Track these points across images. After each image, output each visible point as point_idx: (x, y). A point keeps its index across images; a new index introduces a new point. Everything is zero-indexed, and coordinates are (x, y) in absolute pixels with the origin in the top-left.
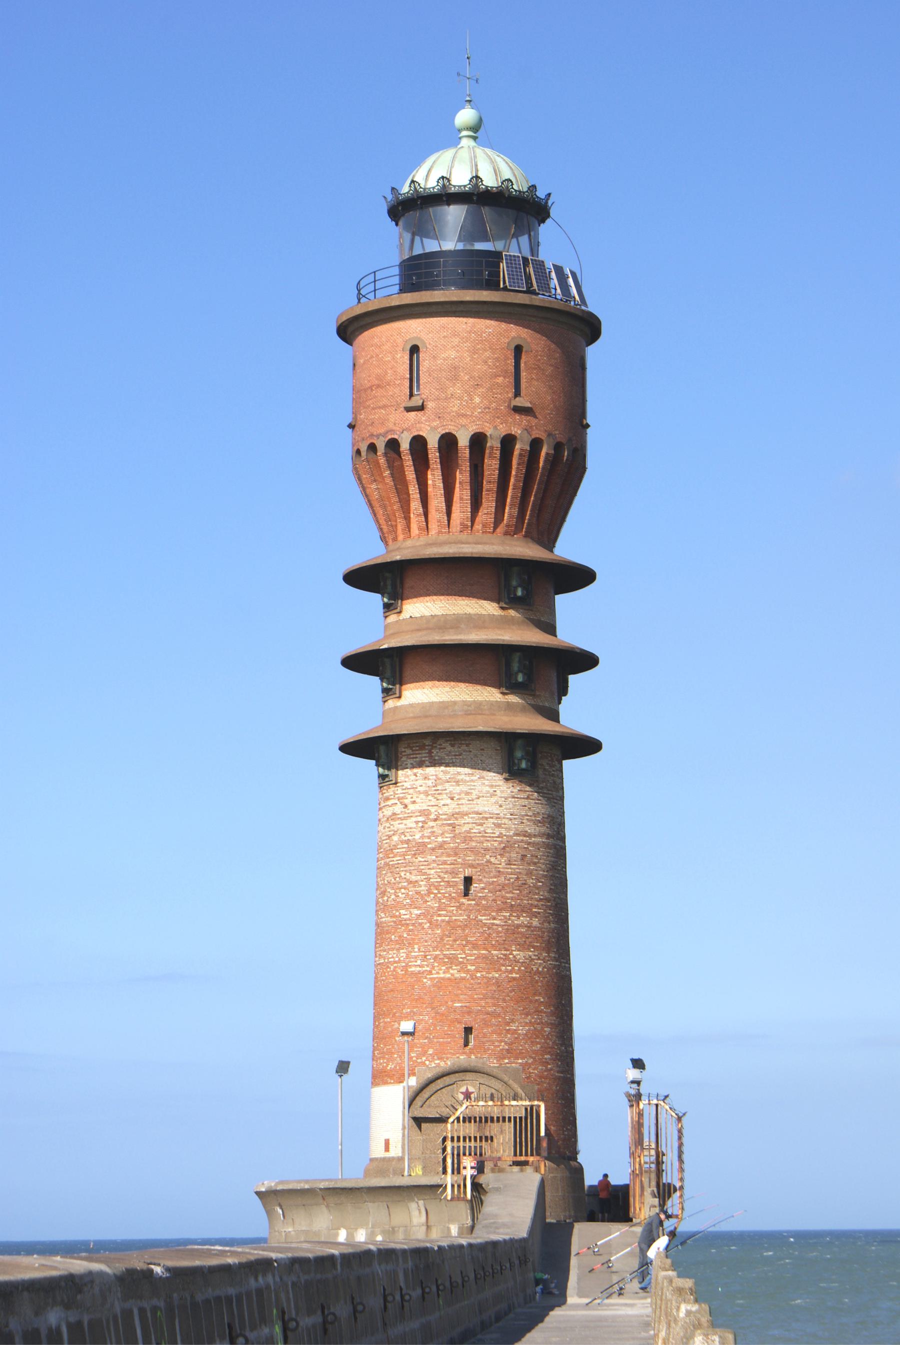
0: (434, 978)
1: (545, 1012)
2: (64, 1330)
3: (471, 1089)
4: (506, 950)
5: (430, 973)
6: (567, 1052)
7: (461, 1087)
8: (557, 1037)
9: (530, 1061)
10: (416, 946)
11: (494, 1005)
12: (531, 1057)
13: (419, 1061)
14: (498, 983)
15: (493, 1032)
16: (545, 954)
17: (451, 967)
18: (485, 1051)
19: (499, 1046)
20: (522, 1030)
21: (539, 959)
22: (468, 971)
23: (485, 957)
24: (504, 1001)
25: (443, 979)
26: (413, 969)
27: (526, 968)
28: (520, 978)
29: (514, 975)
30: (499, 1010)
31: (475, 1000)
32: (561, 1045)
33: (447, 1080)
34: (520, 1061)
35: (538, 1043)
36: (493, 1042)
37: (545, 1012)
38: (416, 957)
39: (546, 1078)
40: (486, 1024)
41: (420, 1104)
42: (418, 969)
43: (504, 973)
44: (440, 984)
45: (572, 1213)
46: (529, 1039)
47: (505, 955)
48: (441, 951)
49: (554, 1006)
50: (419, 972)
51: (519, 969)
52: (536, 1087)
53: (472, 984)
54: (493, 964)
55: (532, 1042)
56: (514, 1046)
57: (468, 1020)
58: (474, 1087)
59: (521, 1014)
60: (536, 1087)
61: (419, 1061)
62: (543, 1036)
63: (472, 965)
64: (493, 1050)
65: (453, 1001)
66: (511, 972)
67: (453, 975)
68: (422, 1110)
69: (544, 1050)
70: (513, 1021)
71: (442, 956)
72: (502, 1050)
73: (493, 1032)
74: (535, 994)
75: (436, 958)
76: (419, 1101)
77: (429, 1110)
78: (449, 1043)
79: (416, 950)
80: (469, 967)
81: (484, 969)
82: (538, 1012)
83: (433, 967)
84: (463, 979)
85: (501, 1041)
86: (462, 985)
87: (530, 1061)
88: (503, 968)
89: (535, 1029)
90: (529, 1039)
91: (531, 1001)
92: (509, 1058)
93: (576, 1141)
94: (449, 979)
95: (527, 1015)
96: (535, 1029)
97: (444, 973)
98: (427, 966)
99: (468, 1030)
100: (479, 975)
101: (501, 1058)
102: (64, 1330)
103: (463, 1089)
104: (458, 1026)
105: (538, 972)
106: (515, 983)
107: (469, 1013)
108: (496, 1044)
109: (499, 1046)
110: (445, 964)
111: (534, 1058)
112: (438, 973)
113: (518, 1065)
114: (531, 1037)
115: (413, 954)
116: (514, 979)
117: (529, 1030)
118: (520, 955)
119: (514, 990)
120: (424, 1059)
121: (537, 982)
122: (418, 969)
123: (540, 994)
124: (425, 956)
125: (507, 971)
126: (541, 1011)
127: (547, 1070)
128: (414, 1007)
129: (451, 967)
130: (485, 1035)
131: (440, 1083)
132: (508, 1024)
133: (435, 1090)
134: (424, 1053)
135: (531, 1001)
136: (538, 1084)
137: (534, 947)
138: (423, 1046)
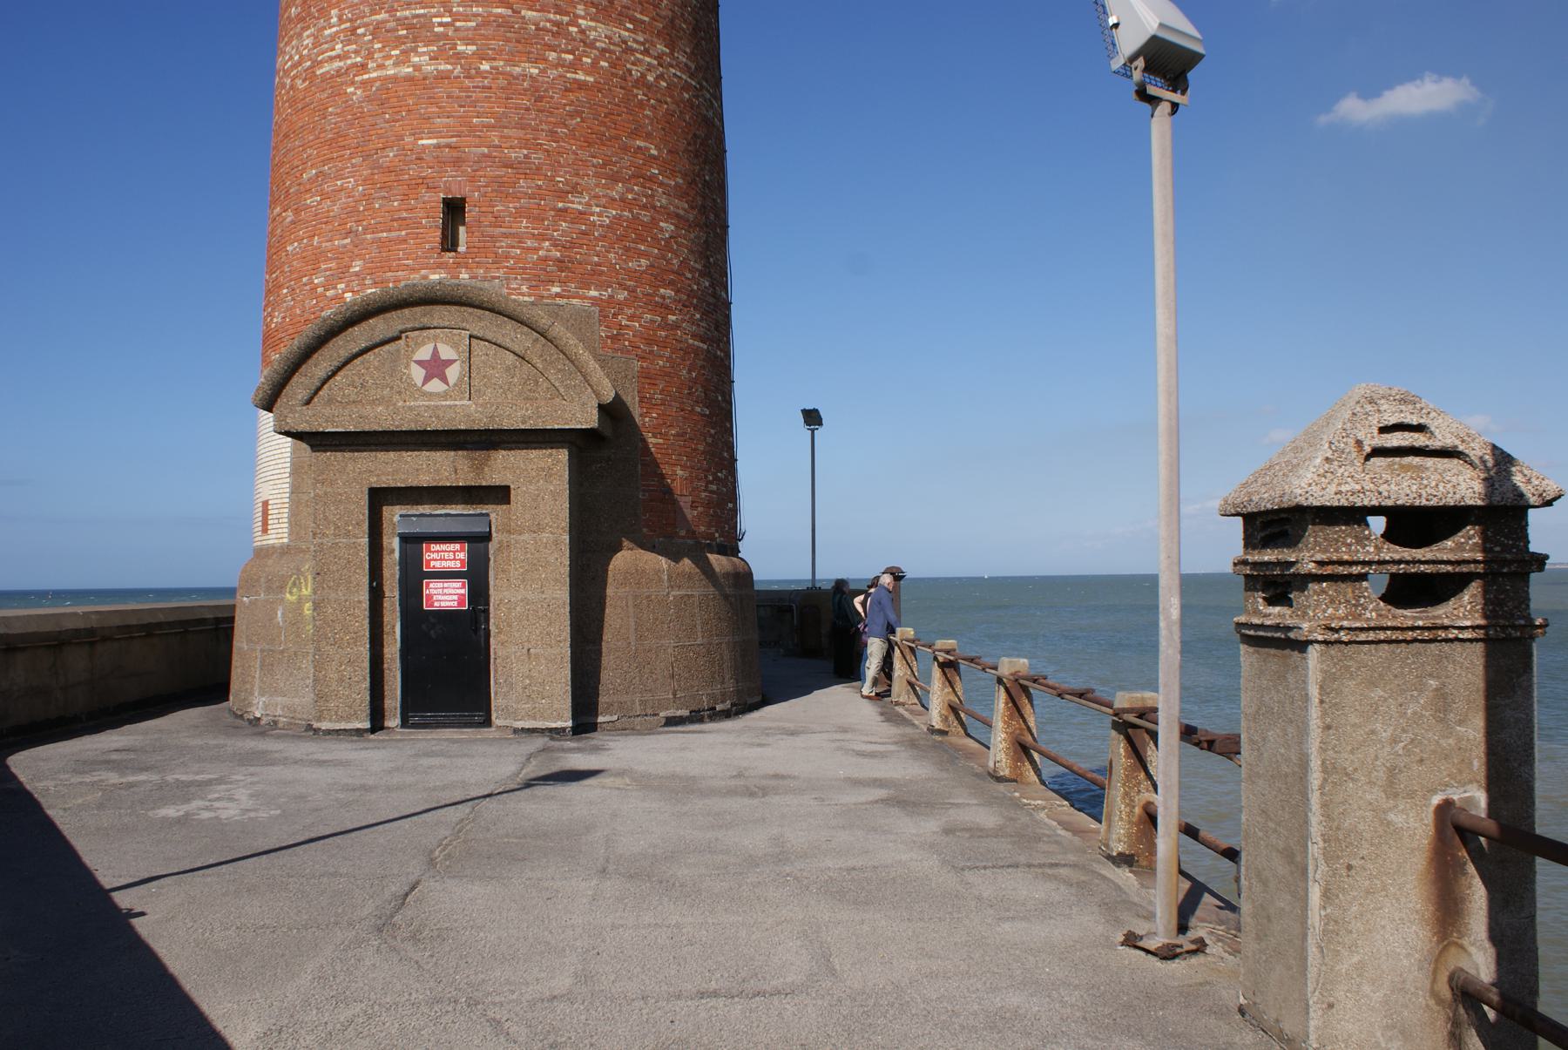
0: (373, 80)
1: (661, 184)
2: (1170, 607)
3: (446, 352)
4: (560, 11)
5: (363, 67)
6: (714, 295)
7: (419, 345)
8: (691, 251)
9: (622, 295)
10: (334, 12)
11: (525, 144)
12: (622, 286)
13: (330, 293)
14: (537, 92)
15: (520, 213)
16: (661, 47)
17: (415, 50)
18: (498, 260)
19: (537, 249)
20: (601, 216)
21: (646, 52)
22: (459, 56)
23: (504, 23)
24: (553, 135)
25: (395, 79)
26: (326, 68)
27: (613, 65)
28: (597, 87)
29: (581, 76)
30: (537, 158)
31: (473, 129)
32: (702, 275)
33: (380, 326)
34: (593, 293)
35: (642, 254)
36: (520, 238)
37: (661, 184)
38: (333, 38)
39: (663, 345)
40: (502, 189)
41: (302, 394)
42: (337, 64)
43: (556, 66)
44: (385, 95)
45: (730, 686)
46: (620, 239)
47: (557, 24)
48: (392, 11)
49: (684, 176)
50: (339, 73)
51: (595, 63)
52: (637, 365)
53: (467, 89)
54: (527, 43)
55: (627, 249)
56: (578, 254)
57: (454, 183)
58: (455, 346)
59: (598, 175)
60: (637, 365)
61: (330, 293)
62: (655, 238)
63: (468, 41)
64: (518, 259)
65: (417, 135)
66: (574, 66)
67: (417, 68)
68: (308, 411)
69: (658, 276)
70: (575, 189)
71: (392, 25)
72: (545, 259)
73: (520, 213)
74: (635, 134)
75: (377, 30)
76: (299, 387)
77: (327, 411)
78: (405, 241)
79: (334, 20)
80: (460, 48)
81: (500, 52)
82: (640, 176)
83: (370, 55)
84: (442, 76)
85: (542, 238)
86: (440, 91)
87: (622, 295)
88: (552, 56)
89: (636, 217)
90: (620, 239)
91: (625, 149)
92: (562, 283)
93: (735, 511)
94: (409, 79)
95: (614, 178)
96: (636, 217)
97: (396, 64)
98: (356, 52)
99: (454, 210)
100: (485, 66)
101: (540, 280)
102: (1170, 607)
103: (424, 353)
104: (427, 196)
105: (641, 82)
106: (582, 96)
107: (457, 163)
108: (529, 243)
109: (537, 249)
110: (400, 41)
111: (632, 291)
112: (381, 67)
113: (587, 303)
114: (628, 234)
115: (327, 32)
116: (581, 86)
117: (619, 218)
118: (599, 32)
119: (578, 113)
120: (341, 286)
121: (641, 104)
122: (337, 64)
123: (648, 137)
124: (353, 30)
125: (560, 64)
126: (652, 179)
127: (665, 325)
128: (324, 163)
129: (415, 50)
130: (498, 221)
131: (359, 336)
132: (562, 195)
133: (344, 354)
134: (343, 272)
135: (625, 149)
136: (642, 358)
137: (633, 20)
138: (339, 254)
